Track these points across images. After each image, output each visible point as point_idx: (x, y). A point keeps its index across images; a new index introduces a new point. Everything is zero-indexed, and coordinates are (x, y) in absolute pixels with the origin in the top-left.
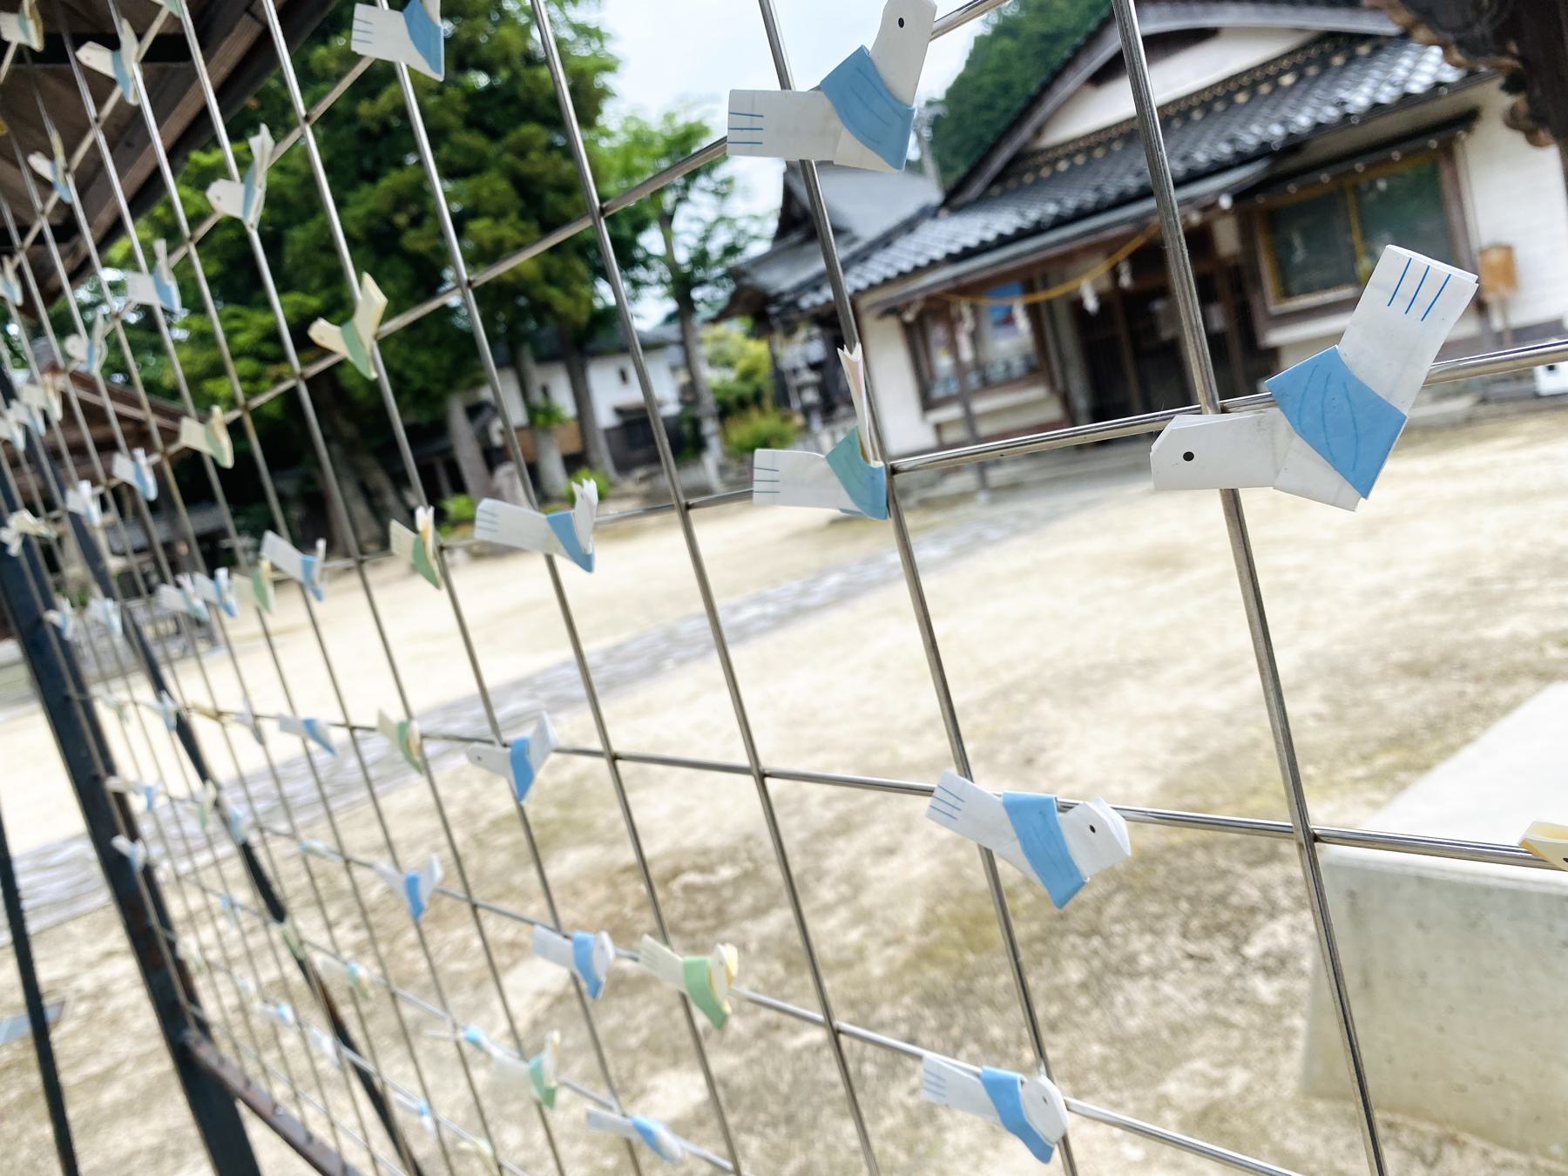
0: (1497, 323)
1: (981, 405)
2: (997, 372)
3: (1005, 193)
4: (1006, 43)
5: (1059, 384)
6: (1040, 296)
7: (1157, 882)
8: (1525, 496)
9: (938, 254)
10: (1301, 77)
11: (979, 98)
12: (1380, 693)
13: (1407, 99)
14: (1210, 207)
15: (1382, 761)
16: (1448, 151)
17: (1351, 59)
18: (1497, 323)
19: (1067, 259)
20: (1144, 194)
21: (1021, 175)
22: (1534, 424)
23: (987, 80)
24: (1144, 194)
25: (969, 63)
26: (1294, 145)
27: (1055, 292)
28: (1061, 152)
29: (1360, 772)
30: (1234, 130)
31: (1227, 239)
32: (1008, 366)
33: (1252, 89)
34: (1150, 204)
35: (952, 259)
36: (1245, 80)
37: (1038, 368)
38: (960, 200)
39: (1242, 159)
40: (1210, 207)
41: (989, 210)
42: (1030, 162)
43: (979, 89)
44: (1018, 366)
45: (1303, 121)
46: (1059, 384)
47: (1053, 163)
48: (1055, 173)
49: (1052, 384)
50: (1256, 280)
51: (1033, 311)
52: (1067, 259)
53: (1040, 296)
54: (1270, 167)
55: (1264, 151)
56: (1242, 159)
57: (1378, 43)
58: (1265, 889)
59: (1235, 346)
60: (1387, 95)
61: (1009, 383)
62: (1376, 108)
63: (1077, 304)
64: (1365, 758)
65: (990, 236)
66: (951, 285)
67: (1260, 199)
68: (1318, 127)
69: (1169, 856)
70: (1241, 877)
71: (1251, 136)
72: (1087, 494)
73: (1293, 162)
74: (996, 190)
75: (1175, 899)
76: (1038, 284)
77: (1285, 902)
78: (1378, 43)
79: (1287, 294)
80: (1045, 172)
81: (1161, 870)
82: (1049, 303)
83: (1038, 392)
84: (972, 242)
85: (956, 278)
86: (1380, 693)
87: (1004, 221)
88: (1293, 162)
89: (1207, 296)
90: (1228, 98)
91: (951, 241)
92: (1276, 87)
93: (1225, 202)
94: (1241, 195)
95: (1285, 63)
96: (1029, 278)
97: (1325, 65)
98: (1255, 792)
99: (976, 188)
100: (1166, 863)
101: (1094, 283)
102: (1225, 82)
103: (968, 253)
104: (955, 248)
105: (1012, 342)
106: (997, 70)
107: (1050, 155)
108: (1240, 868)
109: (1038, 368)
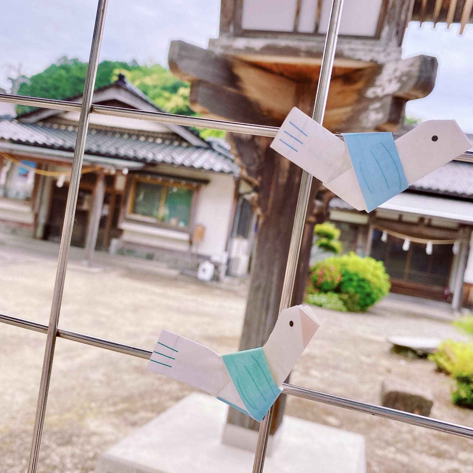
0: (194, 250)
1: (183, 248)
2: (12, 194)
3: (43, 127)
4: (63, 72)
5: (36, 210)
6: (42, 173)
7: (14, 448)
8: (186, 312)
9: (7, 136)
10: (163, 143)
11: (45, 86)
12: (126, 377)
13: (192, 167)
14: (119, 171)
15: (121, 406)
16: (198, 189)
17: (180, 145)
18: (194, 250)
19: (60, 163)
20: (71, 150)
21: (53, 123)
22: (193, 287)
23: (50, 81)
24: (71, 150)
25: (46, 71)
26: (154, 164)
27: (49, 174)
28: (73, 123)
29: (112, 409)
30: (100, 142)
31: (120, 184)
32: (18, 194)
33: (147, 137)
34: (71, 155)
35: (12, 141)
36: (146, 134)
37: (30, 200)
38: (24, 120)
39: (136, 159)
40: (119, 171)
41: (35, 130)
42: (59, 121)
43: (46, 83)
44: (22, 196)
45: (160, 157)
46: (36, 210)
47: (67, 125)
48: (66, 130)
49: (33, 208)
50: (125, 203)
51: (37, 177)
52: (60, 163)
53: (42, 173)
54: (144, 167)
55: (143, 160)
56: (136, 159)
57: (189, 145)
58: (62, 458)
59: (108, 224)
60: (187, 163)
61: (15, 200)
62: (182, 165)
63: (54, 182)
64: (115, 404)
65: (32, 140)
66: (8, 151)
67: (137, 176)
68: (163, 162)
69: (24, 435)
70: (53, 450)
71: (141, 154)
72: (32, 259)
73: (151, 169)
74: (41, 124)
75: (21, 458)
76: (44, 167)
77: (69, 465)
78: (189, 145)
79: (134, 211)
80: (63, 127)
81: (18, 442)
82: (45, 177)
83: (26, 209)
84: (23, 139)
85: (12, 150)
86: (126, 377)
87: (39, 136)
88: (151, 169)
89: (106, 201)
90: (138, 136)
91: (15, 134)
92: (154, 142)
93: (126, 172)
94: (132, 172)
95: (160, 136)
96: (40, 164)
97: (171, 143)
98: (68, 410)
99: (33, 119)
100: (21, 439)
101: (66, 177)
102: (140, 131)
103: (19, 142)
104: (15, 138)
105: (24, 185)
106: (56, 79)
107: (68, 123)
108: (54, 446)
109: (30, 200)
